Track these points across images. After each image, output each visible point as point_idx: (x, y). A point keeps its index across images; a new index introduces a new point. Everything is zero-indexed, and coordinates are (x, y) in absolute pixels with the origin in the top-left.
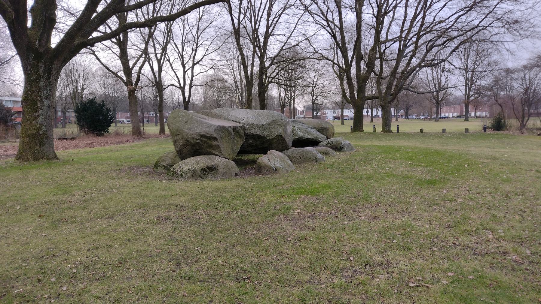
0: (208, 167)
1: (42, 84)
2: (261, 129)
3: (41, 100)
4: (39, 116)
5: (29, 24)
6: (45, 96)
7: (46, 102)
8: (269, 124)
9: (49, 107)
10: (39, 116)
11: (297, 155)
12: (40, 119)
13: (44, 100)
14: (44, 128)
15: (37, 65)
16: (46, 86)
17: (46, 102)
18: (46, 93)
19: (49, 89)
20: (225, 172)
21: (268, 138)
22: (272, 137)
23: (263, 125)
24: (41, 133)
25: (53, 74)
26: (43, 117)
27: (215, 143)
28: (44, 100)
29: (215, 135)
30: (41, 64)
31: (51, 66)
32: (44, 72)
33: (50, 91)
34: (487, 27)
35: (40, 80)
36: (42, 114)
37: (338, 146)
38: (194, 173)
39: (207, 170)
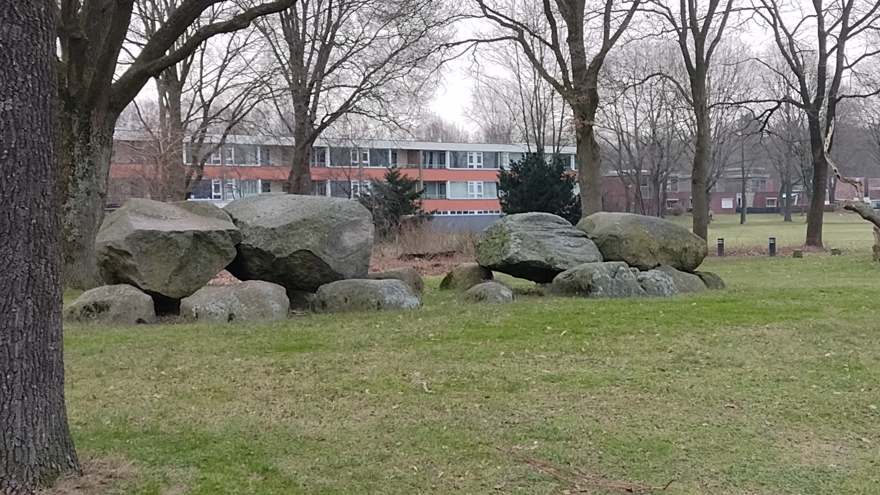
0: (95, 305)
1: (77, 151)
2: (268, 237)
3: (75, 180)
4: (69, 209)
5: (59, 53)
6: (81, 174)
7: (82, 185)
8: (290, 227)
9: (88, 193)
10: (69, 209)
11: (341, 293)
12: (70, 216)
13: (79, 181)
14: (76, 231)
15: (70, 119)
16: (83, 156)
17: (82, 185)
18: (83, 168)
19: (87, 160)
20: (118, 316)
21: (277, 256)
22: (285, 255)
23: (273, 229)
24: (70, 239)
25: (94, 133)
26: (76, 212)
27: (129, 262)
28: (79, 181)
29: (127, 248)
30: (74, 118)
31: (89, 118)
32: (79, 131)
33: (90, 163)
34: (201, 81)
35: (74, 146)
36: (75, 206)
37: (584, 283)
38: (72, 312)
39: (94, 309)
